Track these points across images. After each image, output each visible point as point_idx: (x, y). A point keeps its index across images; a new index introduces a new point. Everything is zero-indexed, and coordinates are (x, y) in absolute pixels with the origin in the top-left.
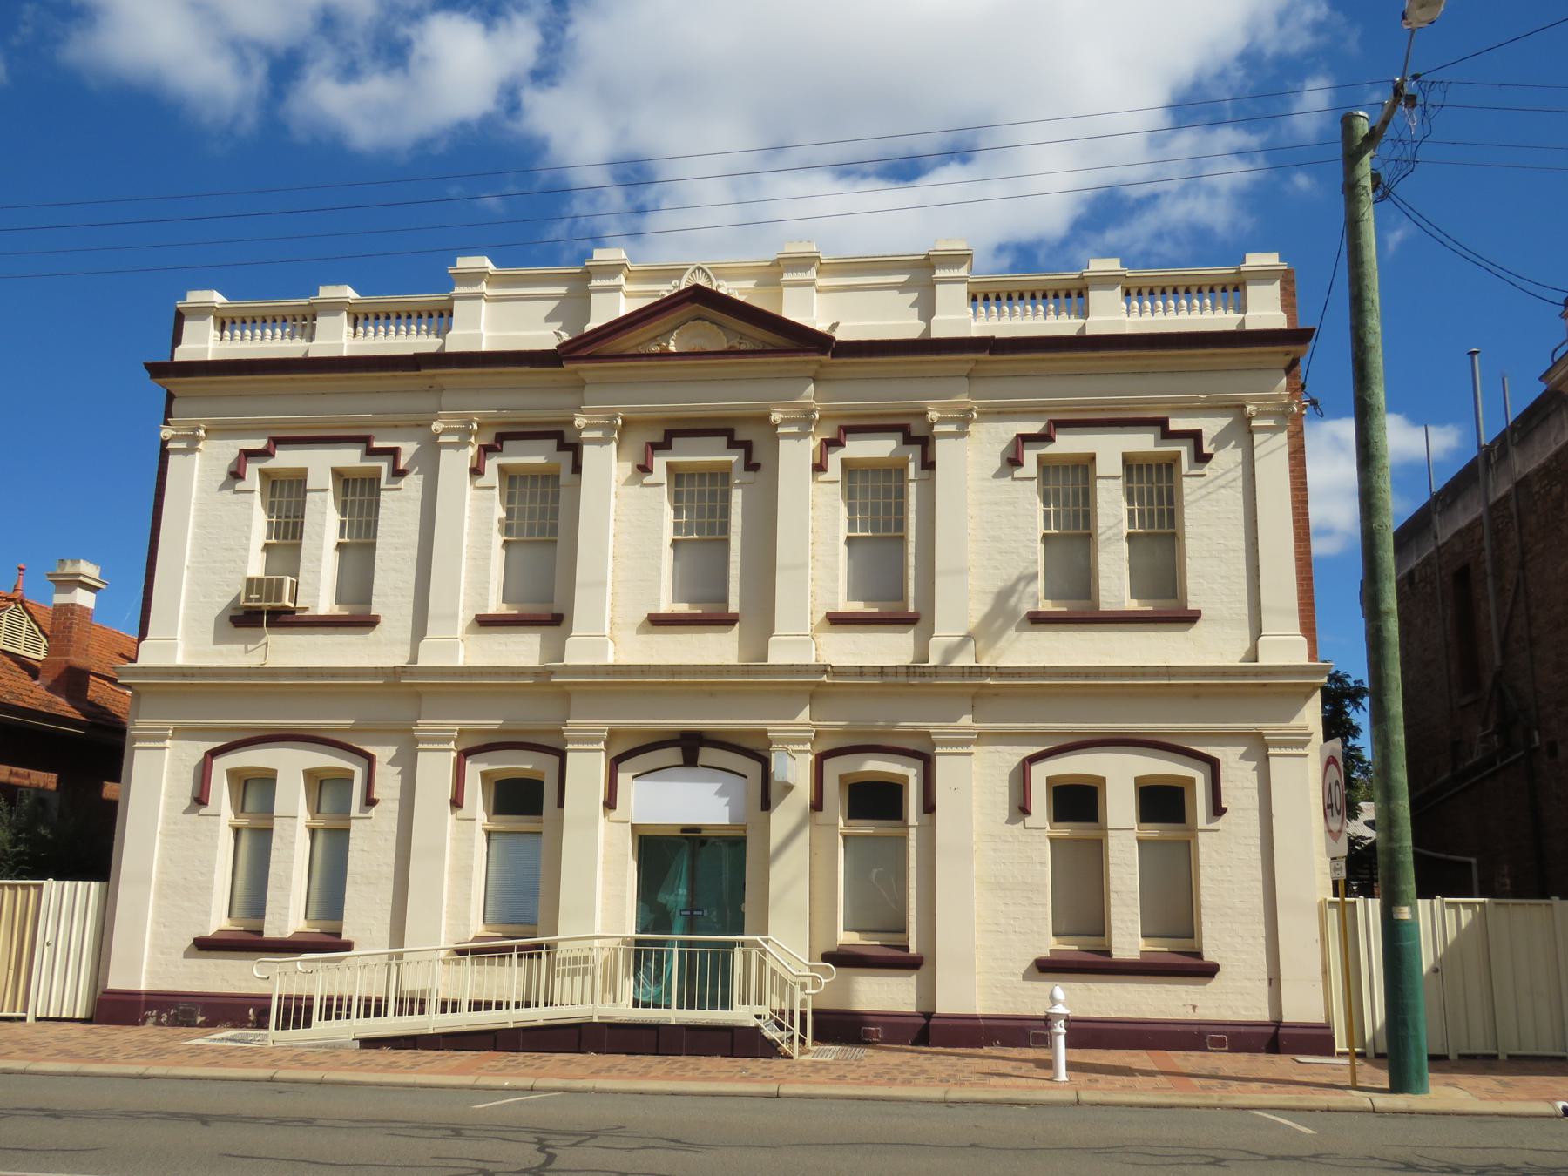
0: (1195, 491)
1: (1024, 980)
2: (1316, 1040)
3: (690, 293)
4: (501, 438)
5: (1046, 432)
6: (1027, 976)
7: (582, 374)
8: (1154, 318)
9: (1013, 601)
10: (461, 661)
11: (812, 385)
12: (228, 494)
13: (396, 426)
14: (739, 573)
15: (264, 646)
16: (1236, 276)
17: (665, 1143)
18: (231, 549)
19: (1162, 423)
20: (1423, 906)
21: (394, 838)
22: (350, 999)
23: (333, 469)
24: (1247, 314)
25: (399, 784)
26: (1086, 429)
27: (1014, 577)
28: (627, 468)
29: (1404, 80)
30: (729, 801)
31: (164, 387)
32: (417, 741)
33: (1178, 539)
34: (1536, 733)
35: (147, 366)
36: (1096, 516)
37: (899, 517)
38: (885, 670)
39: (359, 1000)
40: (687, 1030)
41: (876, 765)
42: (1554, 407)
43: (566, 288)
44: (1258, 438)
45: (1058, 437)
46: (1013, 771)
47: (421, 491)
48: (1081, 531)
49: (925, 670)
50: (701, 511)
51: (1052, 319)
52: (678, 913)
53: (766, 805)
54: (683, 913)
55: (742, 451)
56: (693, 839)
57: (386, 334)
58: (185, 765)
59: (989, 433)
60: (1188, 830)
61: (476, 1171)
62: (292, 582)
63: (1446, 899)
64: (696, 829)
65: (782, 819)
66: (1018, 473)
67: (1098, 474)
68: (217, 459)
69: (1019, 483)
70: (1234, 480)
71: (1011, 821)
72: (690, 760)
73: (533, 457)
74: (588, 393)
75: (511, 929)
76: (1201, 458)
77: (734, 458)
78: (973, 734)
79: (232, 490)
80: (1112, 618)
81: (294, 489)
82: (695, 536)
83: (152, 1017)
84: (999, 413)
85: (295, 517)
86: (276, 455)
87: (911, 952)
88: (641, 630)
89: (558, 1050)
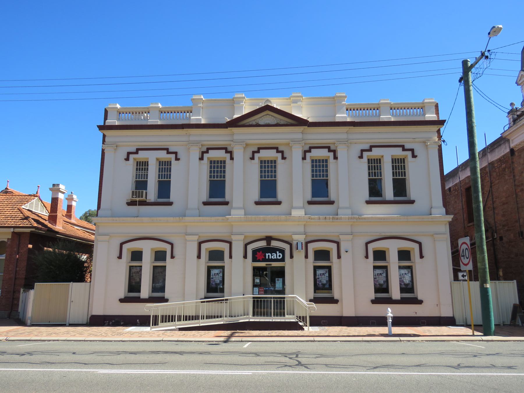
17: (320, 356)
22: (175, 316)
23: (156, 158)
29: (485, 51)
31: (102, 133)
34: (495, 234)
35: (98, 126)
42: (503, 142)
49: (338, 218)
60: (331, 263)
61: (284, 366)
62: (145, 192)
76: (414, 156)
83: (107, 323)
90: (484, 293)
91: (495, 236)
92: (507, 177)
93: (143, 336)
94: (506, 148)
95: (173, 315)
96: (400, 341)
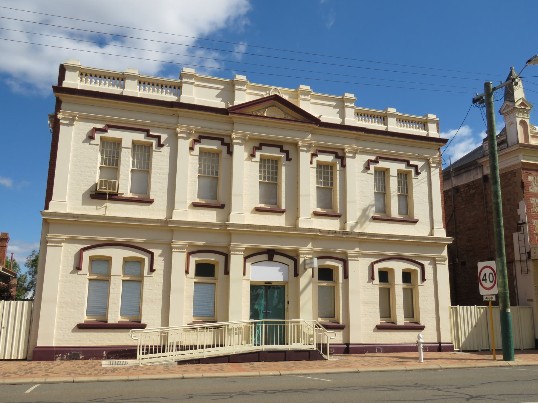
0: (416, 183)
1: (373, 332)
2: (450, 349)
3: (274, 97)
4: (201, 137)
5: (104, 128)
6: (374, 331)
7: (233, 119)
8: (104, 87)
9: (368, 212)
10: (246, 222)
11: (310, 135)
12: (87, 145)
13: (159, 127)
14: (285, 195)
15: (105, 208)
16: (385, 114)
18: (89, 167)
19: (147, 131)
20: (20, 303)
21: (162, 284)
24: (124, 90)
25: (163, 264)
26: (124, 130)
27: (368, 205)
28: (246, 155)
30: (283, 273)
32: (47, 242)
33: (219, 179)
34: (457, 259)
36: (152, 164)
37: (331, 182)
38: (336, 232)
39: (140, 347)
40: (269, 352)
41: (329, 263)
42: (472, 168)
43: (336, 103)
44: (432, 169)
45: (109, 131)
46: (369, 266)
47: (169, 153)
48: (383, 192)
49: (171, 221)
50: (268, 172)
51: (168, 95)
52: (261, 312)
53: (296, 274)
54: (263, 312)
55: (285, 154)
56: (268, 286)
57: (144, 90)
58: (71, 254)
59: (360, 158)
60: (390, 285)
63: (478, 306)
64: (270, 283)
65: (305, 278)
66: (92, 142)
67: (122, 146)
68: (82, 130)
69: (369, 175)
70: (425, 181)
71: (369, 282)
72: (271, 259)
73: (213, 146)
74: (180, 120)
75: (205, 319)
77: (283, 156)
78: (360, 254)
79: (89, 143)
80: (197, 205)
81: (383, 174)
82: (267, 181)
84: (363, 152)
85: (116, 157)
86: (108, 132)
87: (341, 324)
88: (252, 212)
89: (246, 361)
90: (504, 317)
91: (456, 261)
92: (476, 203)
93: (149, 372)
94: (477, 174)
95: (320, 343)
96: (359, 372)
